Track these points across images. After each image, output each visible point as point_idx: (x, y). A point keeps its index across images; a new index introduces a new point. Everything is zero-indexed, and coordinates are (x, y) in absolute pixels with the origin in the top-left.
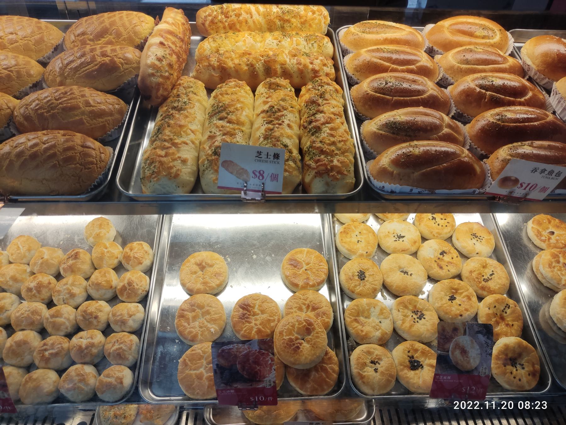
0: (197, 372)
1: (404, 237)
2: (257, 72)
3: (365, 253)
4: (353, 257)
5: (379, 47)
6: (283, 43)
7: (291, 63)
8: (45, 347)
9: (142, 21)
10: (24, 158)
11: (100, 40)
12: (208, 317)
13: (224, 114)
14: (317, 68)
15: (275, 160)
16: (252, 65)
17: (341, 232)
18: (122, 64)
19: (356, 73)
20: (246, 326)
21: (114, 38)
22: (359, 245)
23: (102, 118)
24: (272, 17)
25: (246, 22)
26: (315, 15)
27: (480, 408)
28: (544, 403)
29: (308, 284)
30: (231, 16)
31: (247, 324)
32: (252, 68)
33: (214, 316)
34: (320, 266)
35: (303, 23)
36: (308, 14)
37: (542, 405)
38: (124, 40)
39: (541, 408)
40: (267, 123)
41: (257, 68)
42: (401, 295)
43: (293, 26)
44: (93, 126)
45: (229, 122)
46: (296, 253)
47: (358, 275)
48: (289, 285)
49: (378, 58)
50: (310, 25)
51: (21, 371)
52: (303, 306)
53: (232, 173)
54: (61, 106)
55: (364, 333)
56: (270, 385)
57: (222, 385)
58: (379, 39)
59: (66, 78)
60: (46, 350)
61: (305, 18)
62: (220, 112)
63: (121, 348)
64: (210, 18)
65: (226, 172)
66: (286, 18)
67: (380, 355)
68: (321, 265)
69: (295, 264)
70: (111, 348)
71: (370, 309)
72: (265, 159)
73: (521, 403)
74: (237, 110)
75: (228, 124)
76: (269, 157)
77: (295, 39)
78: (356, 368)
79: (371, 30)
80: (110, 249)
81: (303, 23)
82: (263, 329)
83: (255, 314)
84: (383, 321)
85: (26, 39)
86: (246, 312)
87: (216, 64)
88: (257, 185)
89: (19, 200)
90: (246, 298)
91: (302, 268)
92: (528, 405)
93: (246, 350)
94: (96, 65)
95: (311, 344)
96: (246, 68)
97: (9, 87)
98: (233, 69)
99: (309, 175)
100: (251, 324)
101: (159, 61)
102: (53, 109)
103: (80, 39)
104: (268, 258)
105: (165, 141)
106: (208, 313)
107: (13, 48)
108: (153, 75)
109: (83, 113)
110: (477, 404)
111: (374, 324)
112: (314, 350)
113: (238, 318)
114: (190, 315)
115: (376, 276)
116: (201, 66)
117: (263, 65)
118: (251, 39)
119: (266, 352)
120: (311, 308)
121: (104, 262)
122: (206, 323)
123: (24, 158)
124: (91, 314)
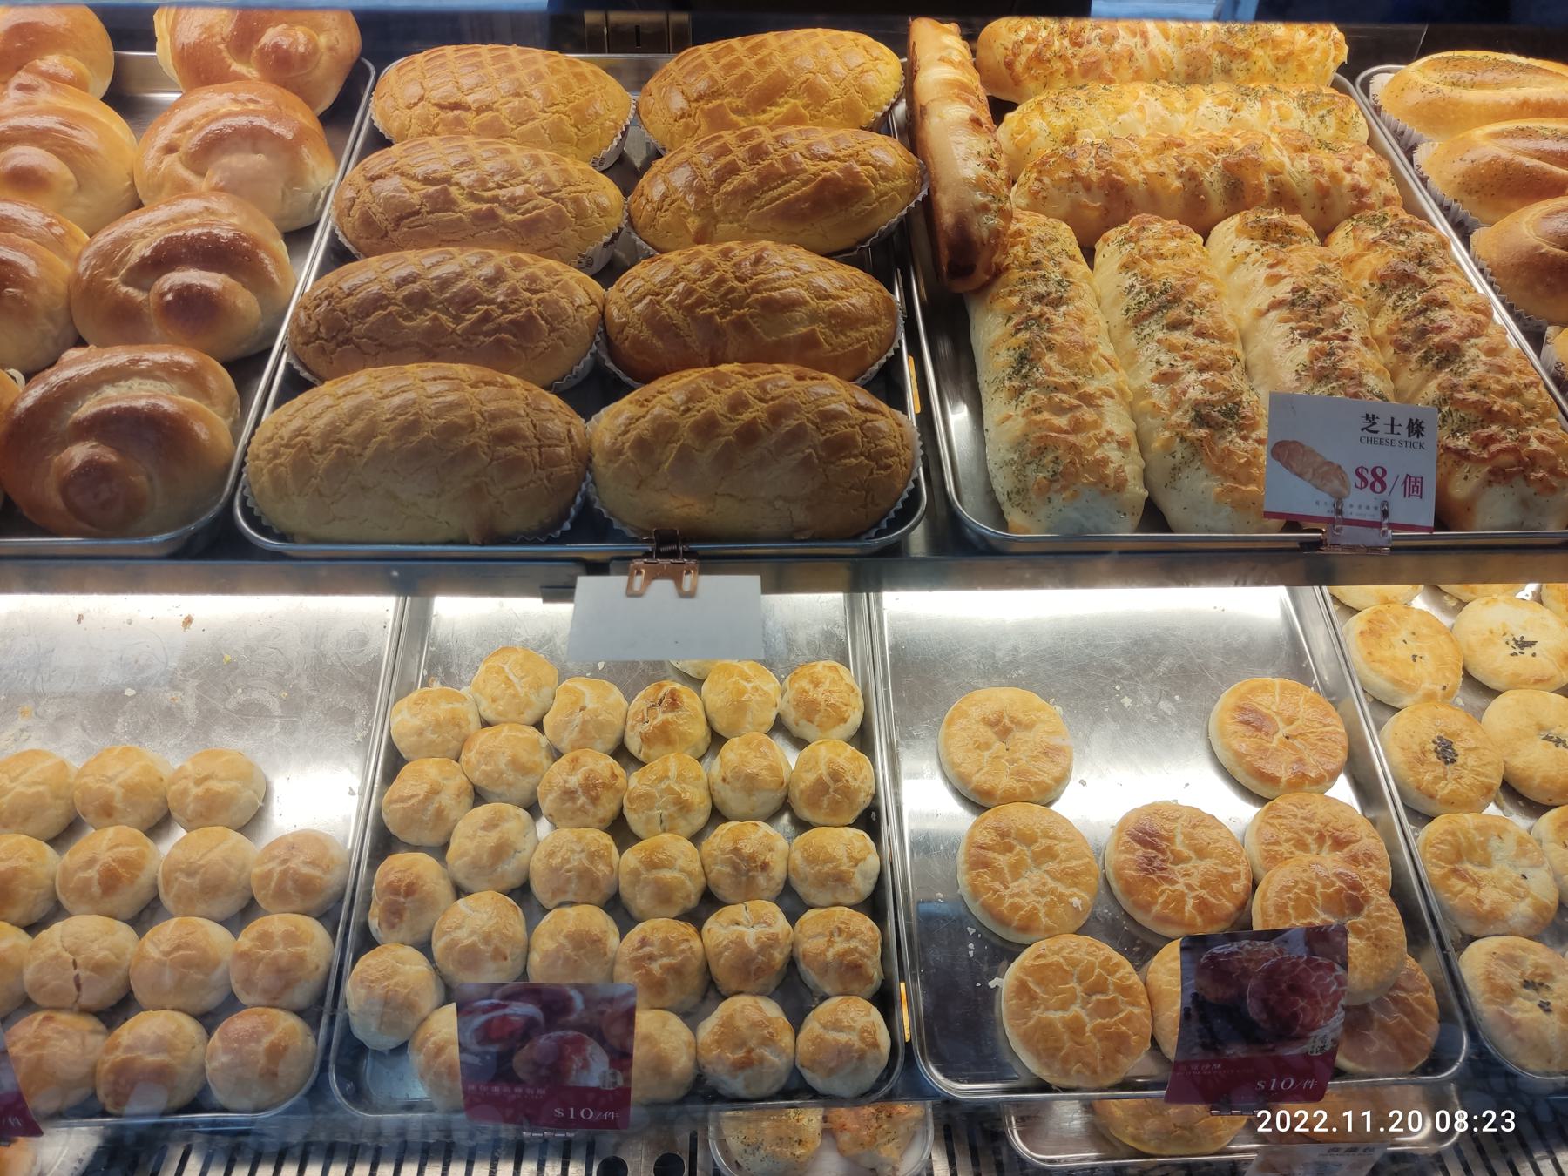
0: (1068, 1015)
1: (1532, 644)
2: (1206, 194)
3: (1438, 688)
4: (1407, 701)
5: (1523, 124)
6: (1244, 113)
7: (1296, 168)
8: (647, 949)
9: (876, 59)
10: (723, 439)
11: (764, 111)
12: (1051, 865)
13: (1178, 312)
14: (1364, 183)
15: (1414, 438)
16: (1191, 177)
17: (1362, 633)
18: (873, 178)
19: (1466, 197)
20: (1163, 892)
21: (806, 107)
22: (1419, 669)
23: (858, 330)
24: (1203, 45)
25: (1131, 56)
26: (1313, 39)
27: (1330, 1129)
28: (1508, 1116)
29: (1304, 776)
30: (1089, 42)
31: (1166, 886)
32: (1193, 184)
33: (1068, 864)
34: (1325, 726)
35: (1281, 61)
36: (1297, 37)
37: (1500, 1121)
38: (834, 111)
39: (1499, 1129)
40: (1303, 336)
41: (1205, 183)
42: (1555, 802)
43: (1255, 69)
44: (840, 351)
45: (1200, 333)
46: (1252, 690)
47: (1436, 751)
48: (1248, 778)
49: (1530, 156)
50: (1302, 67)
51: (89, 1023)
52: (1306, 835)
53: (1300, 475)
54: (756, 296)
55: (1486, 907)
56: (1323, 1048)
57: (1196, 1050)
58: (1504, 102)
59: (716, 219)
60: (651, 958)
61: (1288, 47)
62: (1165, 307)
63: (856, 949)
64: (1032, 47)
65: (1285, 472)
66: (1239, 46)
67: (1546, 966)
68: (1329, 725)
69: (1255, 722)
70: (827, 949)
71: (1487, 840)
72: (1385, 436)
73: (1443, 1117)
74: (1208, 300)
75: (1200, 341)
76: (1396, 429)
77: (1274, 103)
78: (1489, 1001)
79: (1477, 79)
80: (757, 682)
81: (1281, 61)
82: (1213, 900)
83: (1179, 859)
84: (1530, 873)
85: (554, 109)
86: (1154, 853)
87: (1096, 175)
88: (1368, 508)
89: (700, 553)
90: (1155, 810)
91: (1275, 733)
92: (1463, 1120)
93: (1275, 955)
94: (805, 183)
95: (1369, 939)
96: (1177, 184)
97: (557, 245)
98: (1142, 187)
99: (1466, 478)
100: (1177, 887)
101: (991, 169)
102: (739, 303)
103: (706, 107)
104: (1165, 706)
105: (1057, 388)
106: (1049, 854)
107: (522, 135)
108: (985, 208)
109: (814, 317)
110: (1321, 1116)
111: (1507, 883)
112: (1380, 955)
113: (1137, 870)
114: (1003, 861)
115: (1487, 752)
116: (1046, 180)
117: (1223, 176)
118: (1158, 103)
119: (1327, 962)
120: (1329, 842)
121: (749, 717)
122: (1052, 884)
123: (723, 439)
124: (751, 858)
